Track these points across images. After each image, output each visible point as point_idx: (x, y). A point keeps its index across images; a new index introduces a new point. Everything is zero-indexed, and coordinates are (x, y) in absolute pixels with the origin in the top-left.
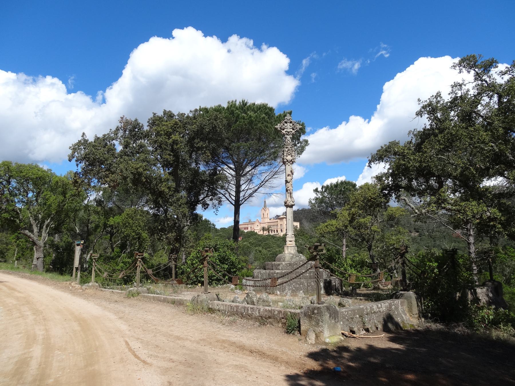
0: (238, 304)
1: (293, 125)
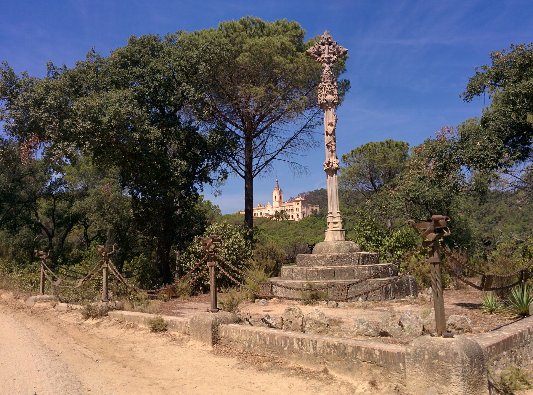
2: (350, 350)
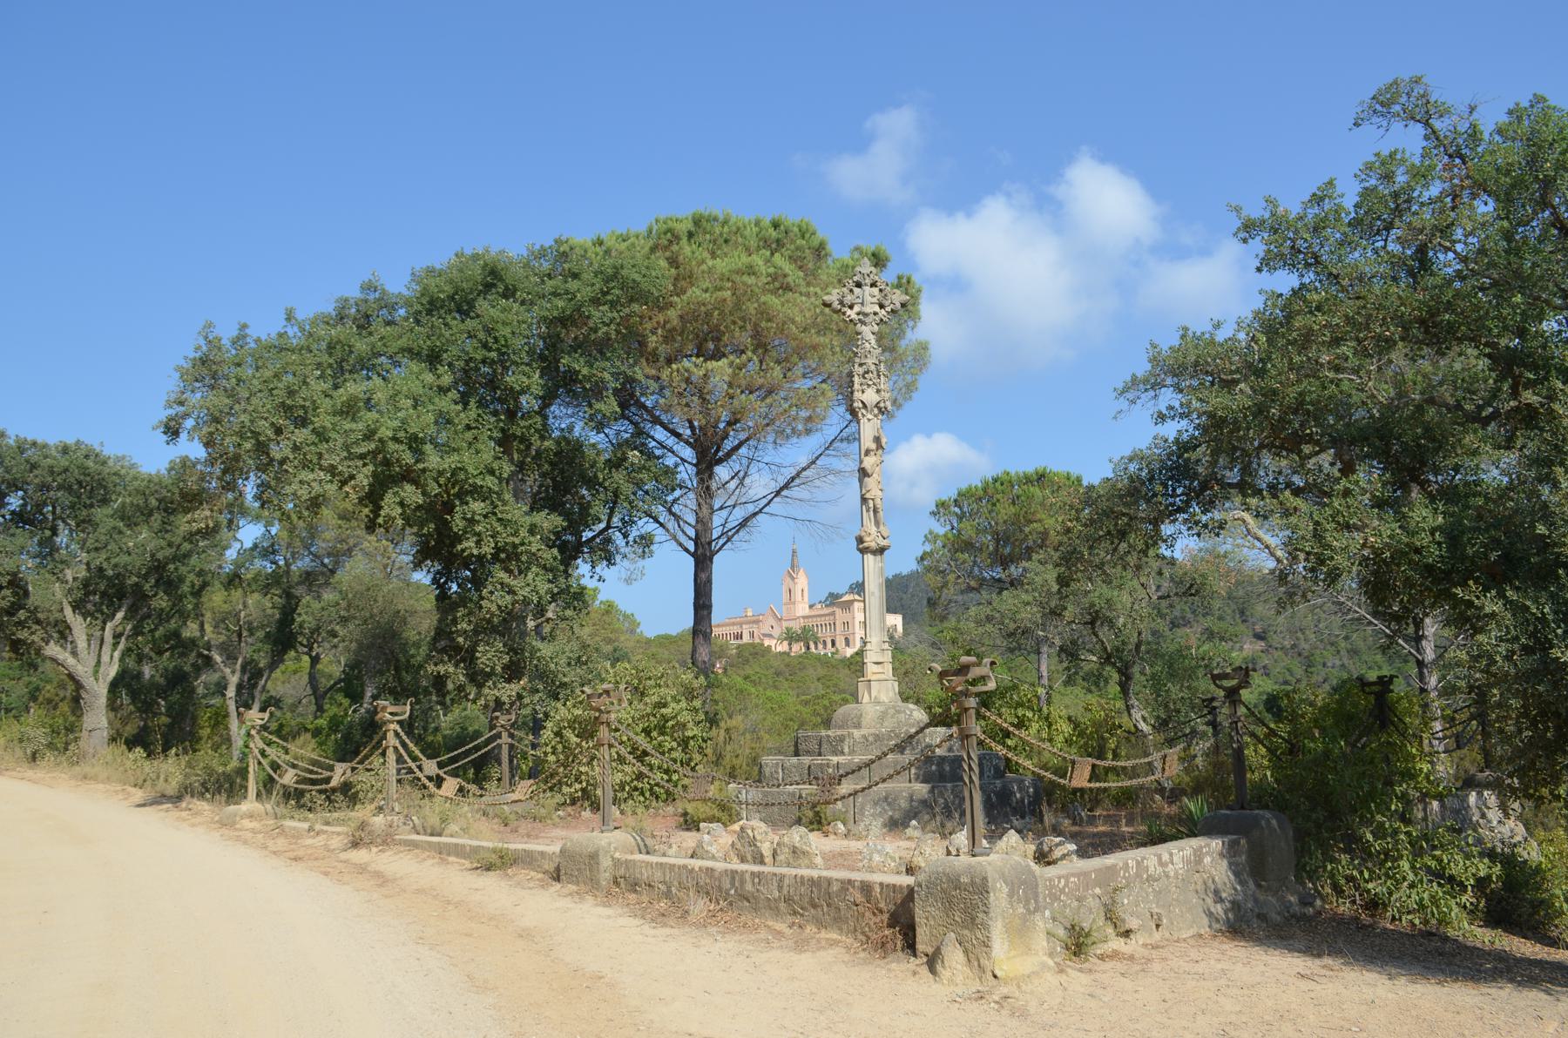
0: (709, 864)
2: (835, 887)
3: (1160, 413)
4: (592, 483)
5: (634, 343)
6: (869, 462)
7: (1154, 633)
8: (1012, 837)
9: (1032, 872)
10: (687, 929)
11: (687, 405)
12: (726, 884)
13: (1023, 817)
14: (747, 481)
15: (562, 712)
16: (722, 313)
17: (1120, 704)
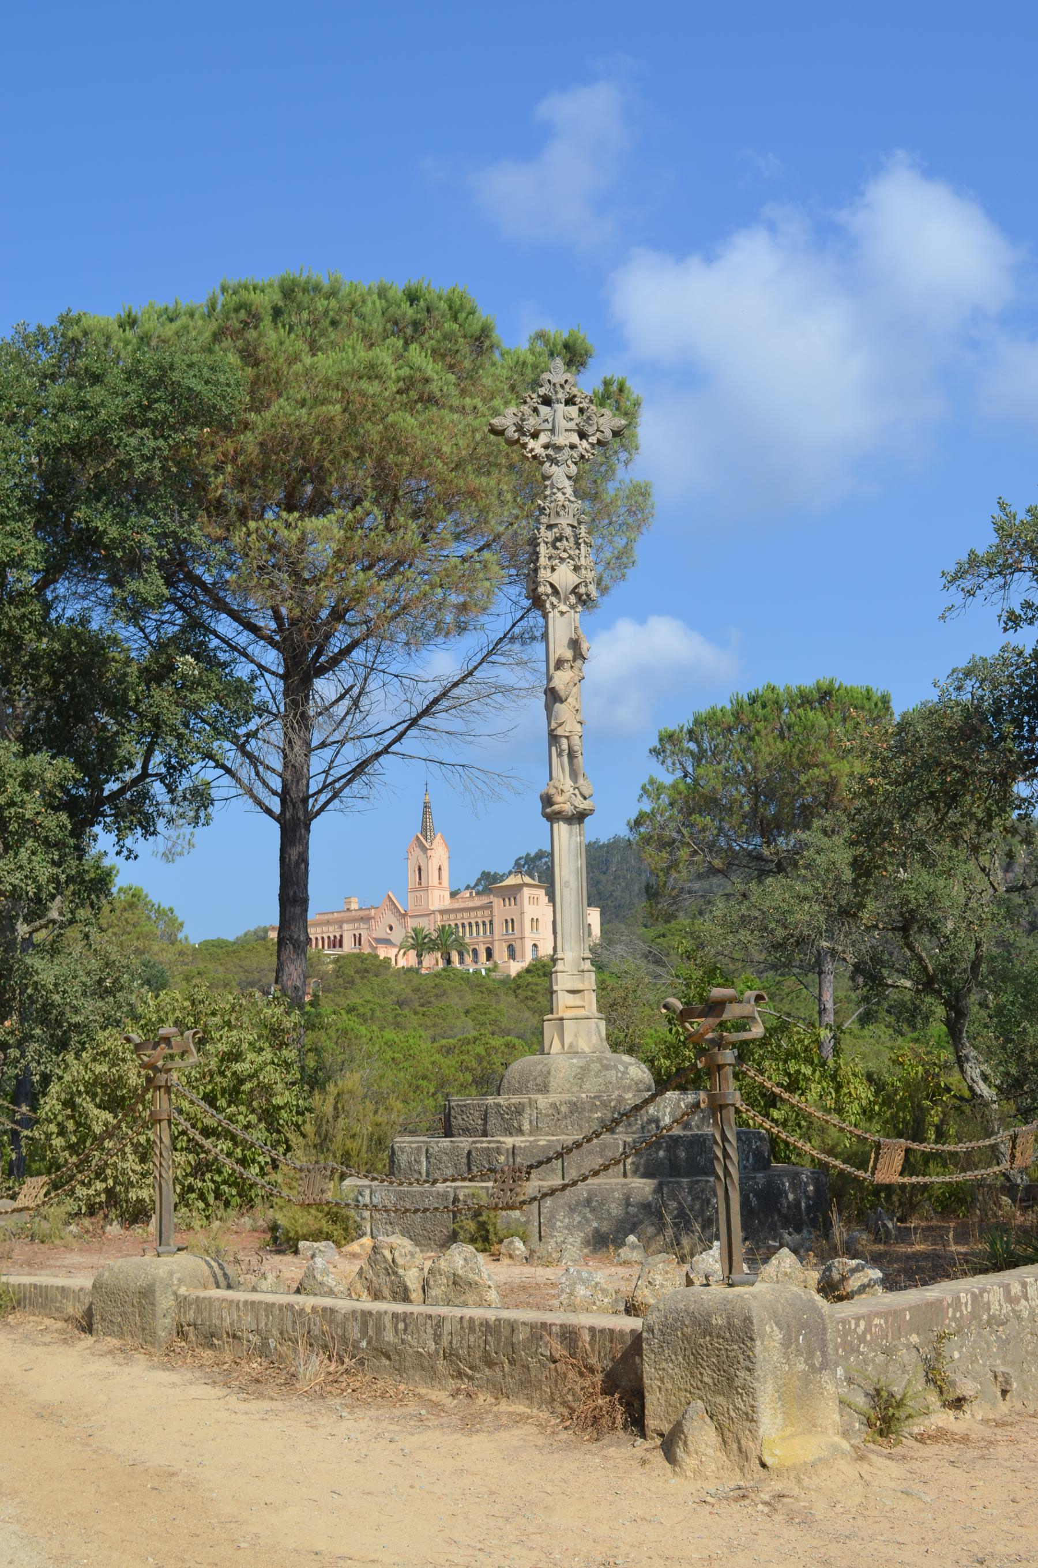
0: (328, 1302)
1: (581, 411)
2: (522, 1335)
3: (1012, 613)
4: (118, 705)
5: (188, 487)
6: (561, 679)
7: (1002, 943)
8: (785, 1260)
9: (816, 1310)
10: (295, 1401)
11: (272, 585)
12: (355, 1333)
13: (798, 1230)
14: (364, 701)
15: (76, 1069)
16: (327, 441)
17: (947, 1055)
